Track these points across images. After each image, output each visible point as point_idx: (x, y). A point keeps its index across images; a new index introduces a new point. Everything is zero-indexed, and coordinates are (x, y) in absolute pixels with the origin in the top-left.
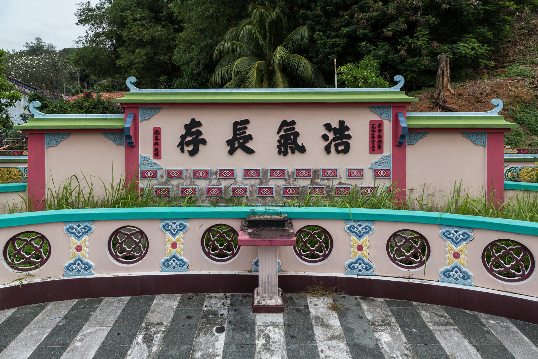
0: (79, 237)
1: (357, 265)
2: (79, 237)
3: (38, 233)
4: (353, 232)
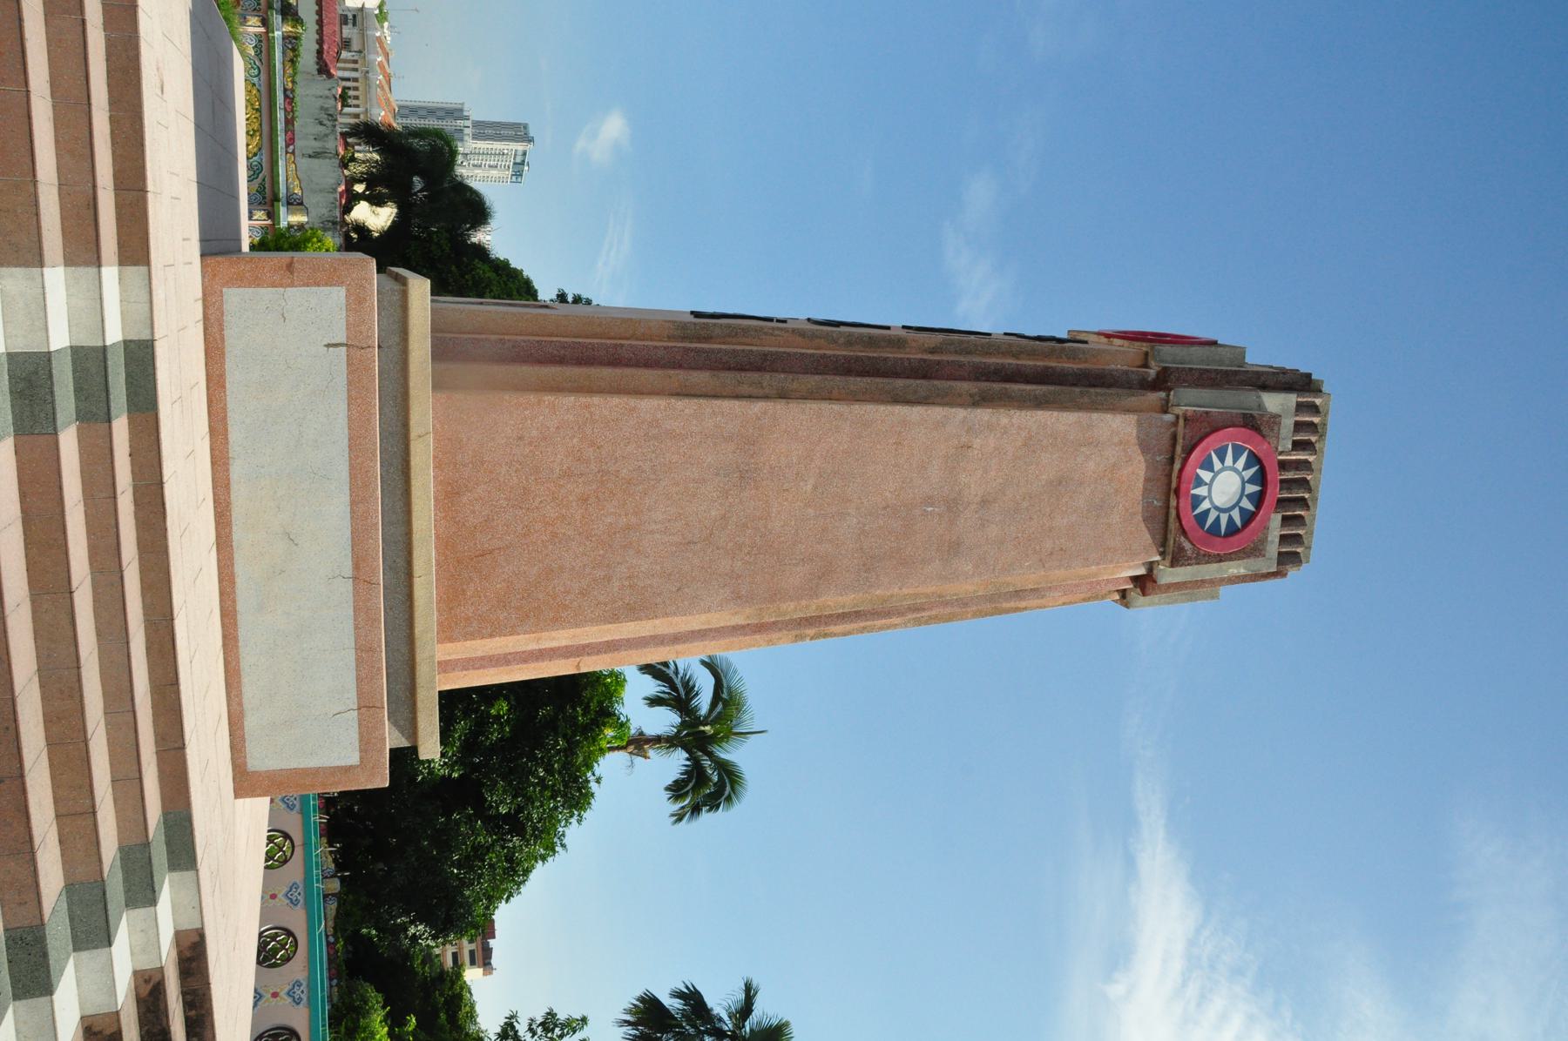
0: (286, 895)
1: (295, 995)
2: (286, 895)
3: (291, 857)
4: (294, 986)
